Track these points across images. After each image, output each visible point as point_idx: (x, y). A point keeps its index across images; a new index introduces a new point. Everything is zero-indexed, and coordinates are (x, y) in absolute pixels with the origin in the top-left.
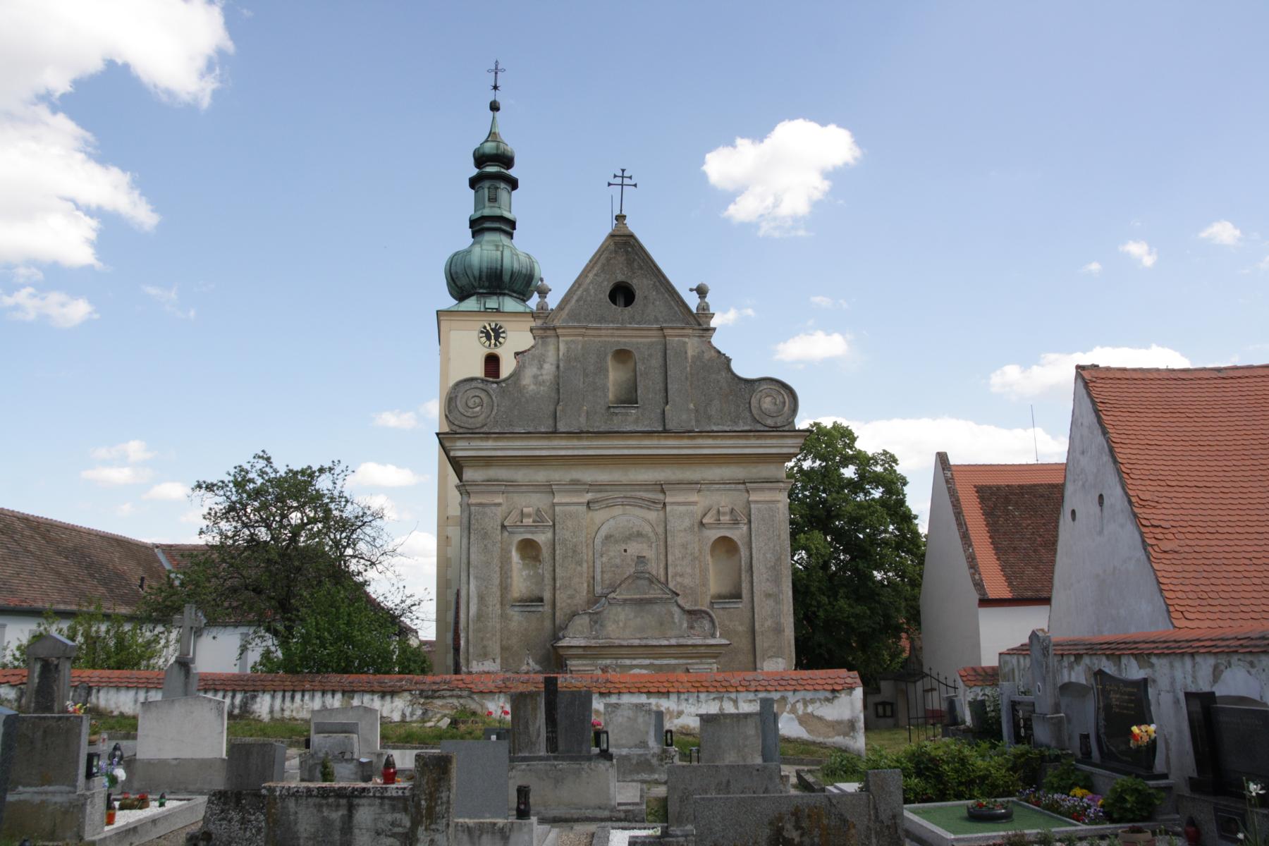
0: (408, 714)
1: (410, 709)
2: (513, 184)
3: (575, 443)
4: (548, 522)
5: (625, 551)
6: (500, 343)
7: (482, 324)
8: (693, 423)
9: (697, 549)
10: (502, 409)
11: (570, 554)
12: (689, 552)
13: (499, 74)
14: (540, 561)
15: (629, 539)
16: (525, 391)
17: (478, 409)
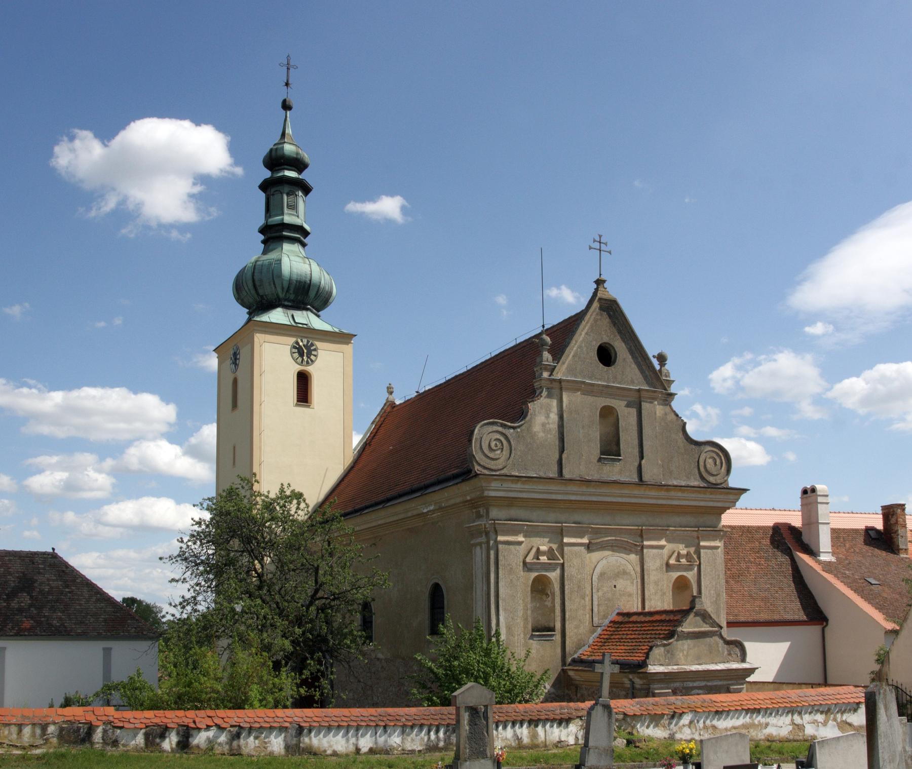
2: (307, 190)
3: (584, 489)
5: (615, 586)
6: (312, 361)
7: (294, 340)
9: (665, 586)
10: (519, 453)
11: (576, 589)
12: (659, 587)
13: (291, 70)
14: (547, 594)
16: (536, 438)
17: (499, 452)
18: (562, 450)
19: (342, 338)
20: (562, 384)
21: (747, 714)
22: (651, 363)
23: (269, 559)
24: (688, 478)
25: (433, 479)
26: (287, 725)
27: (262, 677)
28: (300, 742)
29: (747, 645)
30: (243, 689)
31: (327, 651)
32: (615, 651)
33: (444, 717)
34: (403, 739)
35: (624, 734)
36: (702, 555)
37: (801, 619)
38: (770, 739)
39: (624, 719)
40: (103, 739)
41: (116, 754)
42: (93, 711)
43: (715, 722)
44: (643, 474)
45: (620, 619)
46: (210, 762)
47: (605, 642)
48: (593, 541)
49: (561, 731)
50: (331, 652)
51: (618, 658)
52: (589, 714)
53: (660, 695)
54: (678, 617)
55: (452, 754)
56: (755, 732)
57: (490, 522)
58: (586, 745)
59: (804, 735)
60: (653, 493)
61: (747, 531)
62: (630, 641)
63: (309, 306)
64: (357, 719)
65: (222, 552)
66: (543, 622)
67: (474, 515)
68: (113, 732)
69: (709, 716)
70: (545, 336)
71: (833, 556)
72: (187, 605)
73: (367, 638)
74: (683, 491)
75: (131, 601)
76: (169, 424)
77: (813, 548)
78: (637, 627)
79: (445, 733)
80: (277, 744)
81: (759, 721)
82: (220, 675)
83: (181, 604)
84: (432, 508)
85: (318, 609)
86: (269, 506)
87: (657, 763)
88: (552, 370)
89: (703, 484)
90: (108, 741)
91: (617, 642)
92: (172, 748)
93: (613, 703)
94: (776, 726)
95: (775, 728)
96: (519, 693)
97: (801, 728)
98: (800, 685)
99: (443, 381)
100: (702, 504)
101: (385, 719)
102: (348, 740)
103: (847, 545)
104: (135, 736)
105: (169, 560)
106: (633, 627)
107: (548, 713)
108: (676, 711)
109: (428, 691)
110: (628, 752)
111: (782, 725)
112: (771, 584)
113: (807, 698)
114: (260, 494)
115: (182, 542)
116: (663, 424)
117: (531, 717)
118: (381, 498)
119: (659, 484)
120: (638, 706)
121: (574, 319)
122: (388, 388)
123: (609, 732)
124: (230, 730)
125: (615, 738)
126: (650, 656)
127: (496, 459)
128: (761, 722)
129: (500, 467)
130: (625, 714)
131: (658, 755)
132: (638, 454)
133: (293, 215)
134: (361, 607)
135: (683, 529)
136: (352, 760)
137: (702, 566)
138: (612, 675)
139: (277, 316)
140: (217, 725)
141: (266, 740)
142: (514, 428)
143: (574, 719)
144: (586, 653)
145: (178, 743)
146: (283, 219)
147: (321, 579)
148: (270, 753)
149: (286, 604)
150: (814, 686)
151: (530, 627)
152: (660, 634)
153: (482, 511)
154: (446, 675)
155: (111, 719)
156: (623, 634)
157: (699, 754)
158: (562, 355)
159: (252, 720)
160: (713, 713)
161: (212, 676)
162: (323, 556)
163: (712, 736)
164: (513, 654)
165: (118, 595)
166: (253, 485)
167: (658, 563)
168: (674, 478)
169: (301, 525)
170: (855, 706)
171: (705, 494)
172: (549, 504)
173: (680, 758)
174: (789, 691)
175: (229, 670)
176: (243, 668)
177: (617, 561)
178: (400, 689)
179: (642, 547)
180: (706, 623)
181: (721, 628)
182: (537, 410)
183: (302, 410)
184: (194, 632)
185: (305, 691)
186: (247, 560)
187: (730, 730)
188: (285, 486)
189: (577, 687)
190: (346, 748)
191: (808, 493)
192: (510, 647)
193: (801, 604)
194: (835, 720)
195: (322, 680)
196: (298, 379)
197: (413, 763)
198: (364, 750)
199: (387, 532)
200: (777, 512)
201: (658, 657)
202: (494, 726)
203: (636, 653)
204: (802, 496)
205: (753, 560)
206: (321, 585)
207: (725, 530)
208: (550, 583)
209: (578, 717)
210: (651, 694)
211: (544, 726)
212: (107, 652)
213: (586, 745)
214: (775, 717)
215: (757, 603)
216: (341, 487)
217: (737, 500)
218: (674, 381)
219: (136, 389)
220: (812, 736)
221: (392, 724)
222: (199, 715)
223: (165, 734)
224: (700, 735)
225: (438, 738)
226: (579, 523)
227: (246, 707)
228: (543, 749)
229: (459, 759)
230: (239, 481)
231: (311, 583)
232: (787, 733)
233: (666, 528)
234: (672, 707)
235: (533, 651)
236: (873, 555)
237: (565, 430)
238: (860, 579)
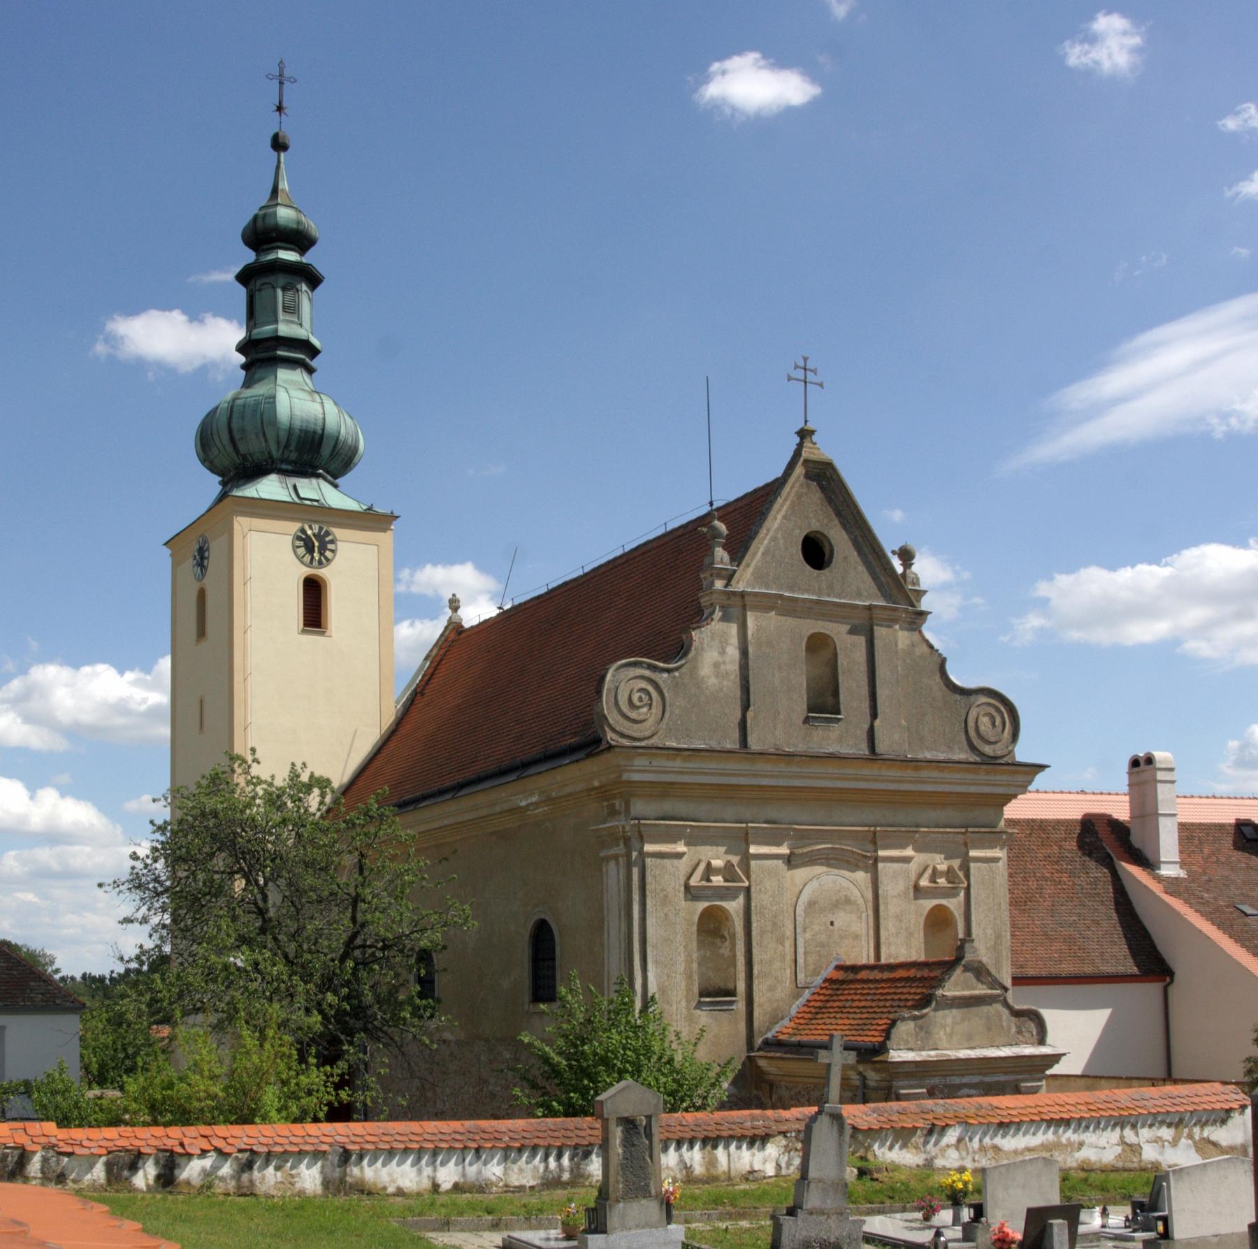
0: (783, 1165)
1: (786, 1158)
2: (314, 280)
3: (782, 767)
4: (741, 881)
5: (832, 923)
6: (328, 560)
7: (297, 526)
9: (913, 921)
10: (677, 712)
11: (769, 928)
12: (903, 925)
13: (287, 85)
14: (723, 937)
15: (836, 906)
17: (645, 710)
18: (746, 706)
19: (372, 520)
20: (747, 598)
21: (1049, 1127)
24: (950, 748)
26: (325, 1147)
28: (345, 1174)
29: (1048, 1014)
32: (835, 1027)
33: (569, 1133)
36: (972, 871)
38: (1086, 1168)
40: (43, 1172)
42: (25, 1129)
43: (998, 1141)
44: (876, 742)
45: (840, 975)
47: (817, 1013)
48: (797, 851)
49: (753, 1155)
52: (809, 1129)
53: (908, 1097)
54: (937, 973)
56: (1063, 1156)
57: (632, 822)
59: (1141, 1161)
62: (857, 1011)
63: (321, 471)
66: (718, 982)
67: (606, 811)
69: (989, 1131)
70: (717, 523)
71: (1181, 868)
78: (869, 988)
79: (571, 1159)
80: (310, 1177)
81: (1068, 1140)
84: (534, 799)
86: (274, 800)
87: (908, 1205)
88: (729, 577)
89: (973, 758)
90: (50, 1176)
91: (836, 1012)
92: (148, 1186)
94: (1096, 1147)
95: (1094, 1150)
98: (1129, 1080)
99: (543, 590)
100: (973, 789)
101: (477, 1138)
102: (420, 1171)
103: (1206, 851)
104: (91, 1167)
105: (114, 888)
106: (863, 988)
107: (733, 1127)
108: (936, 1122)
110: (860, 1188)
111: (1106, 1145)
112: (1079, 915)
113: (1146, 1103)
116: (908, 661)
117: (705, 1133)
118: (448, 783)
119: (902, 758)
120: (875, 1115)
121: (762, 493)
124: (237, 1157)
126: (892, 1036)
127: (641, 722)
128: (1072, 1139)
129: (647, 733)
131: (909, 1192)
132: (868, 710)
133: (292, 322)
135: (941, 830)
137: (972, 891)
138: (845, 1068)
139: (270, 488)
140: (217, 1150)
141: (293, 1172)
142: (668, 671)
143: (774, 1136)
144: (785, 1031)
145: (158, 1177)
146: (276, 330)
148: (299, 1192)
150: (1156, 1083)
151: (696, 989)
152: (907, 1000)
153: (618, 804)
155: (53, 1140)
156: (847, 1000)
157: (979, 1191)
158: (746, 553)
159: (271, 1142)
160: (995, 1126)
166: (249, 767)
168: (927, 748)
170: (1223, 1115)
172: (726, 793)
173: (947, 1196)
174: (1116, 1091)
178: (481, 1090)
179: (876, 860)
181: (1006, 989)
182: (706, 641)
185: (348, 1095)
188: (298, 767)
189: (771, 1085)
190: (417, 1183)
191: (1141, 765)
193: (1130, 948)
194: (1190, 1136)
196: (304, 589)
197: (525, 1206)
198: (446, 1185)
199: (458, 838)
201: (905, 1036)
203: (869, 1030)
204: (1130, 769)
205: (1048, 875)
208: (727, 919)
209: (780, 1133)
210: (893, 1096)
211: (727, 1147)
214: (1094, 1131)
215: (1057, 946)
216: (377, 763)
218: (925, 592)
220: (1153, 1163)
221: (489, 1145)
222: (187, 1134)
223: (137, 1163)
224: (974, 1160)
225: (560, 1166)
226: (774, 822)
227: (257, 1120)
228: (726, 1183)
229: (607, 1199)
232: (1112, 1157)
233: (914, 829)
234: (930, 1116)
236: (1249, 867)
237: (751, 672)
238: (1227, 907)
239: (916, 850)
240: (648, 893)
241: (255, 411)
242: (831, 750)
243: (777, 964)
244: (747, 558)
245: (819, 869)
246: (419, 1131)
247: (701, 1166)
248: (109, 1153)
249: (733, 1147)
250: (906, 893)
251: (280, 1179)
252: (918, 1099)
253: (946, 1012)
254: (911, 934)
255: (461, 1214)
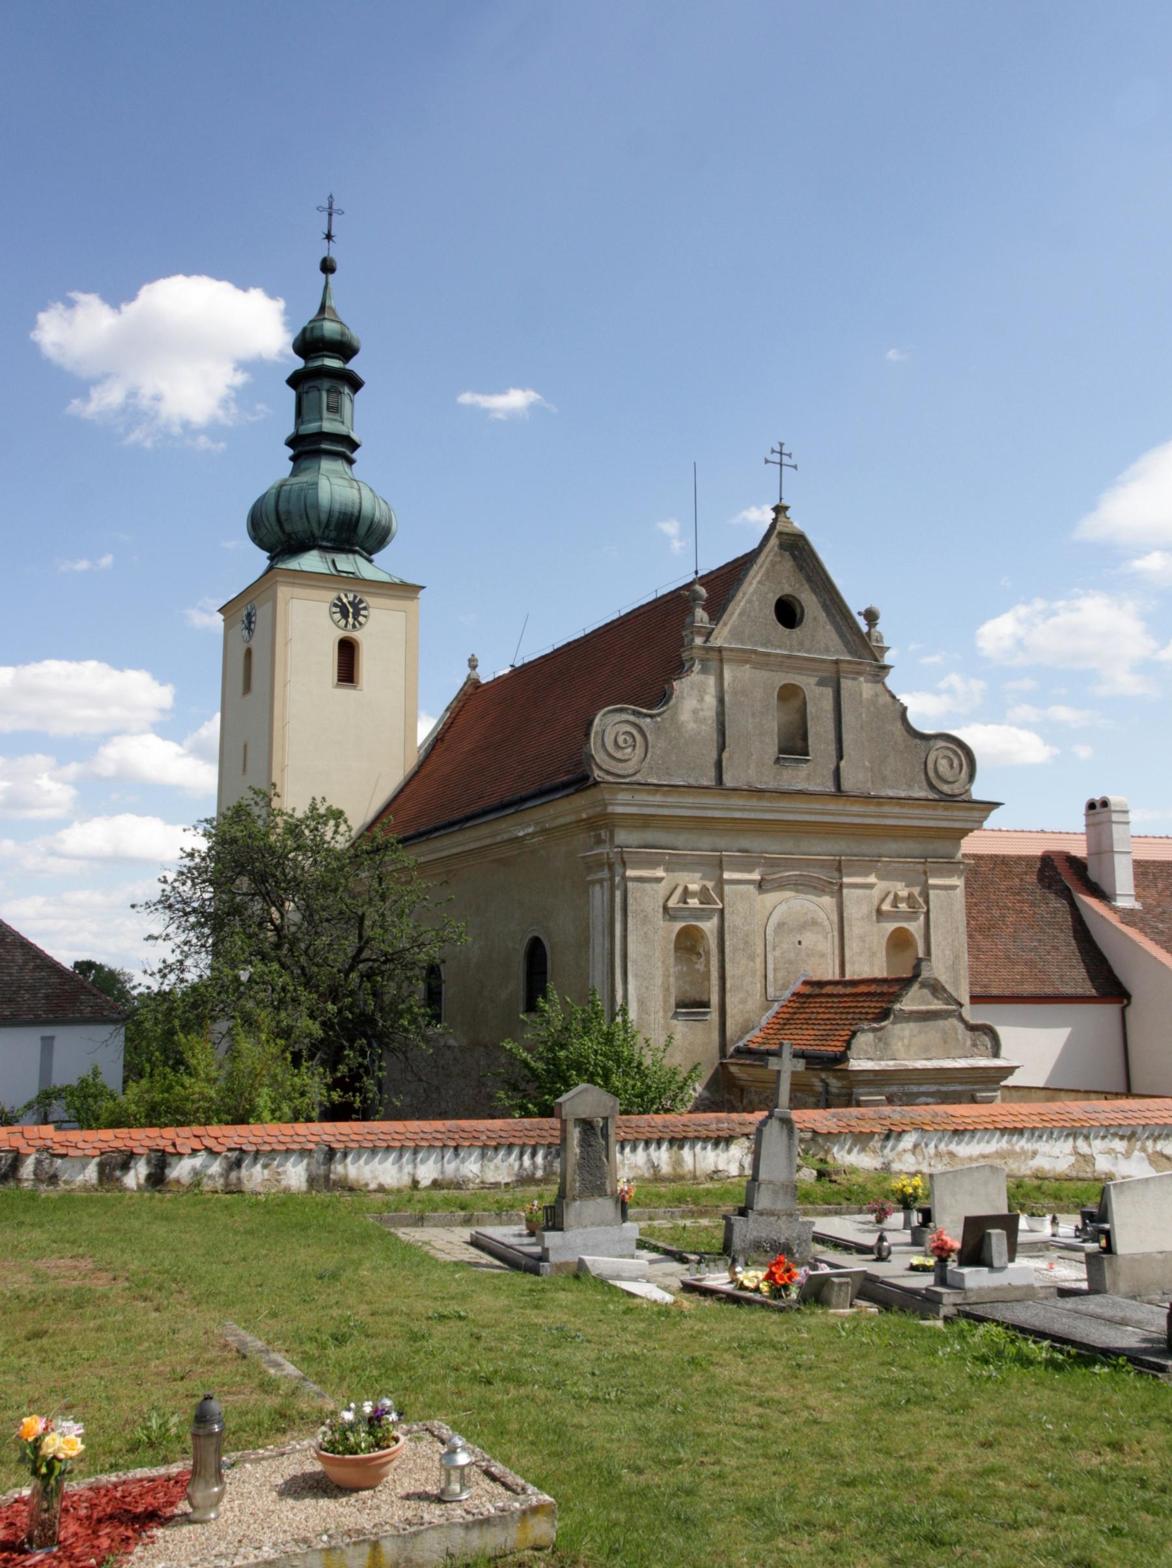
2: (355, 384)
3: (754, 802)
5: (800, 943)
6: (360, 624)
8: (870, 785)
10: (658, 752)
11: (741, 946)
14: (699, 954)
17: (629, 750)
18: (722, 747)
20: (724, 653)
21: (1003, 1135)
22: (855, 622)
23: (292, 904)
25: (532, 790)
26: (311, 1146)
27: (276, 1075)
28: (329, 1171)
29: (1002, 1031)
30: (246, 1094)
31: (374, 1036)
33: (544, 1133)
34: (482, 1166)
35: (814, 1161)
36: (931, 897)
37: (1088, 993)
38: (1040, 1176)
39: (813, 1139)
40: (35, 1174)
41: (54, 1195)
43: (953, 1147)
44: (842, 780)
45: (807, 990)
46: (195, 1205)
48: (767, 877)
49: (718, 1156)
50: (381, 1038)
51: (804, 1047)
52: (759, 1131)
53: (868, 1104)
54: (895, 989)
55: (555, 1188)
58: (755, 1178)
60: (857, 808)
61: (1001, 862)
64: (415, 1137)
65: (224, 896)
66: (694, 995)
68: (51, 1164)
70: (698, 587)
72: (170, 972)
73: (433, 1017)
74: (902, 806)
75: (85, 967)
76: (162, 711)
77: (1105, 886)
79: (545, 1158)
80: (295, 1175)
81: (1022, 1148)
82: (214, 1074)
83: (160, 971)
84: (530, 830)
85: (362, 976)
86: (293, 830)
88: (708, 635)
89: (932, 796)
92: (139, 1186)
93: (795, 1115)
96: (655, 1098)
97: (1088, 1159)
98: (1088, 1093)
99: (549, 650)
100: (931, 824)
102: (401, 1169)
103: (1160, 885)
104: (84, 1167)
108: (893, 1128)
109: (521, 1094)
110: (819, 1189)
112: (1040, 941)
113: (1097, 1115)
114: (281, 813)
115: (165, 882)
116: (872, 709)
118: (457, 816)
122: (470, 661)
123: (790, 1159)
124: (226, 1157)
125: (799, 1168)
126: (853, 1046)
127: (625, 761)
129: (631, 772)
130: (814, 1132)
134: (424, 972)
136: (407, 1198)
139: (311, 561)
141: (280, 1170)
142: (651, 716)
143: (737, 1138)
144: (755, 1040)
145: (149, 1177)
146: (321, 427)
147: (368, 933)
149: (315, 969)
151: (672, 1001)
152: (867, 1013)
153: (604, 834)
154: (548, 1071)
155: (49, 1143)
159: (260, 1140)
161: (203, 1075)
162: (371, 899)
163: (949, 1169)
164: (647, 1041)
165: (66, 958)
166: (271, 800)
167: (865, 909)
169: (343, 852)
171: (935, 809)
172: (702, 824)
174: (1069, 1103)
175: (228, 1066)
176: (245, 1064)
177: (802, 906)
178: (480, 1092)
179: (841, 886)
180: (938, 998)
181: (961, 1005)
183: (346, 693)
184: (179, 1012)
186: (259, 907)
187: (976, 1159)
188: (318, 801)
189: (742, 1090)
192: (643, 1031)
194: (1143, 1149)
195: (365, 1079)
197: (497, 1202)
198: (425, 1182)
200: (1047, 836)
202: (618, 1148)
206: (367, 942)
207: (967, 861)
208: (702, 937)
209: (743, 1135)
211: (693, 1148)
212: (48, 1041)
213: (755, 1178)
215: (1019, 968)
217: (985, 818)
218: (888, 648)
219: (120, 664)
221: (467, 1144)
225: (534, 1165)
226: (747, 851)
227: (251, 1120)
229: (564, 1198)
230: (250, 794)
231: (353, 938)
232: (1066, 1166)
234: (887, 1122)
235: (677, 1037)
237: (727, 718)
239: (878, 877)
240: (629, 914)
241: (299, 495)
242: (800, 788)
243: (748, 979)
244: (725, 617)
245: (788, 894)
246: (402, 1130)
247: (668, 1165)
248: (102, 1154)
249: (699, 1146)
250: (869, 916)
251: (266, 1177)
252: (878, 1105)
253: (904, 1025)
254: (873, 954)
255: (435, 1210)
